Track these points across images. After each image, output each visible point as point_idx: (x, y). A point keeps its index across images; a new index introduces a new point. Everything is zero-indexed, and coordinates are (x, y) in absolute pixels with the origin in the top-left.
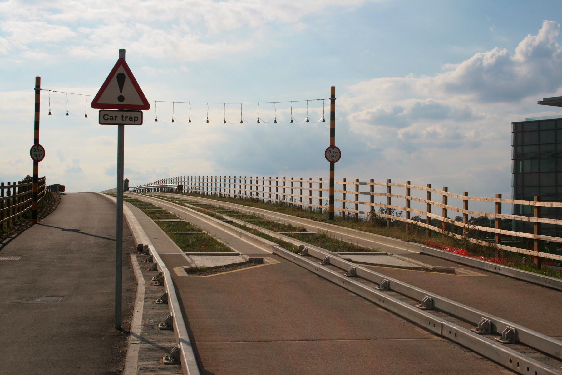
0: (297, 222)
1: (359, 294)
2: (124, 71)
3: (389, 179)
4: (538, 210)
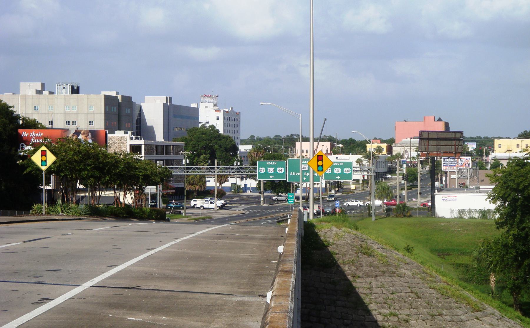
0: (197, 215)
3: (54, 92)
4: (192, 103)
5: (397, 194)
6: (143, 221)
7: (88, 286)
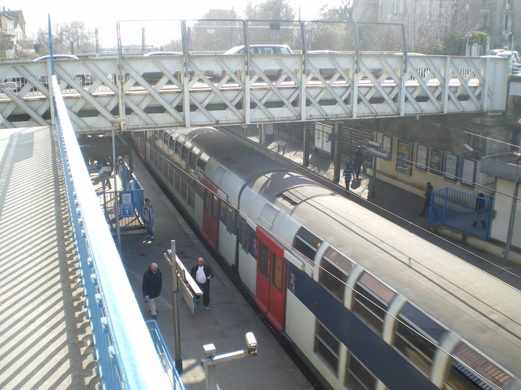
2: (240, 46)
5: (292, 218)
6: (445, 373)
7: (209, 264)
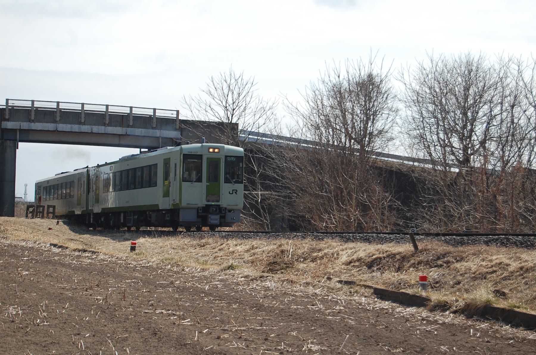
1: (182, 188)
3: (165, 160)
6: (48, 182)
